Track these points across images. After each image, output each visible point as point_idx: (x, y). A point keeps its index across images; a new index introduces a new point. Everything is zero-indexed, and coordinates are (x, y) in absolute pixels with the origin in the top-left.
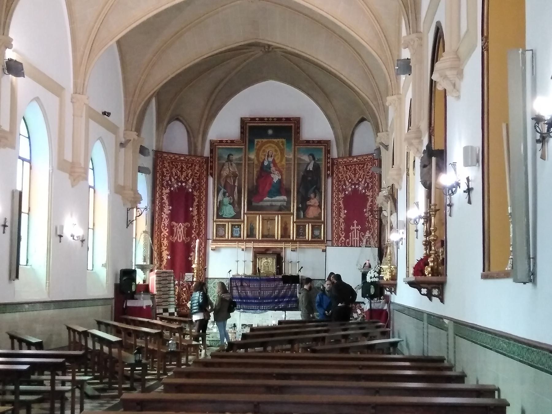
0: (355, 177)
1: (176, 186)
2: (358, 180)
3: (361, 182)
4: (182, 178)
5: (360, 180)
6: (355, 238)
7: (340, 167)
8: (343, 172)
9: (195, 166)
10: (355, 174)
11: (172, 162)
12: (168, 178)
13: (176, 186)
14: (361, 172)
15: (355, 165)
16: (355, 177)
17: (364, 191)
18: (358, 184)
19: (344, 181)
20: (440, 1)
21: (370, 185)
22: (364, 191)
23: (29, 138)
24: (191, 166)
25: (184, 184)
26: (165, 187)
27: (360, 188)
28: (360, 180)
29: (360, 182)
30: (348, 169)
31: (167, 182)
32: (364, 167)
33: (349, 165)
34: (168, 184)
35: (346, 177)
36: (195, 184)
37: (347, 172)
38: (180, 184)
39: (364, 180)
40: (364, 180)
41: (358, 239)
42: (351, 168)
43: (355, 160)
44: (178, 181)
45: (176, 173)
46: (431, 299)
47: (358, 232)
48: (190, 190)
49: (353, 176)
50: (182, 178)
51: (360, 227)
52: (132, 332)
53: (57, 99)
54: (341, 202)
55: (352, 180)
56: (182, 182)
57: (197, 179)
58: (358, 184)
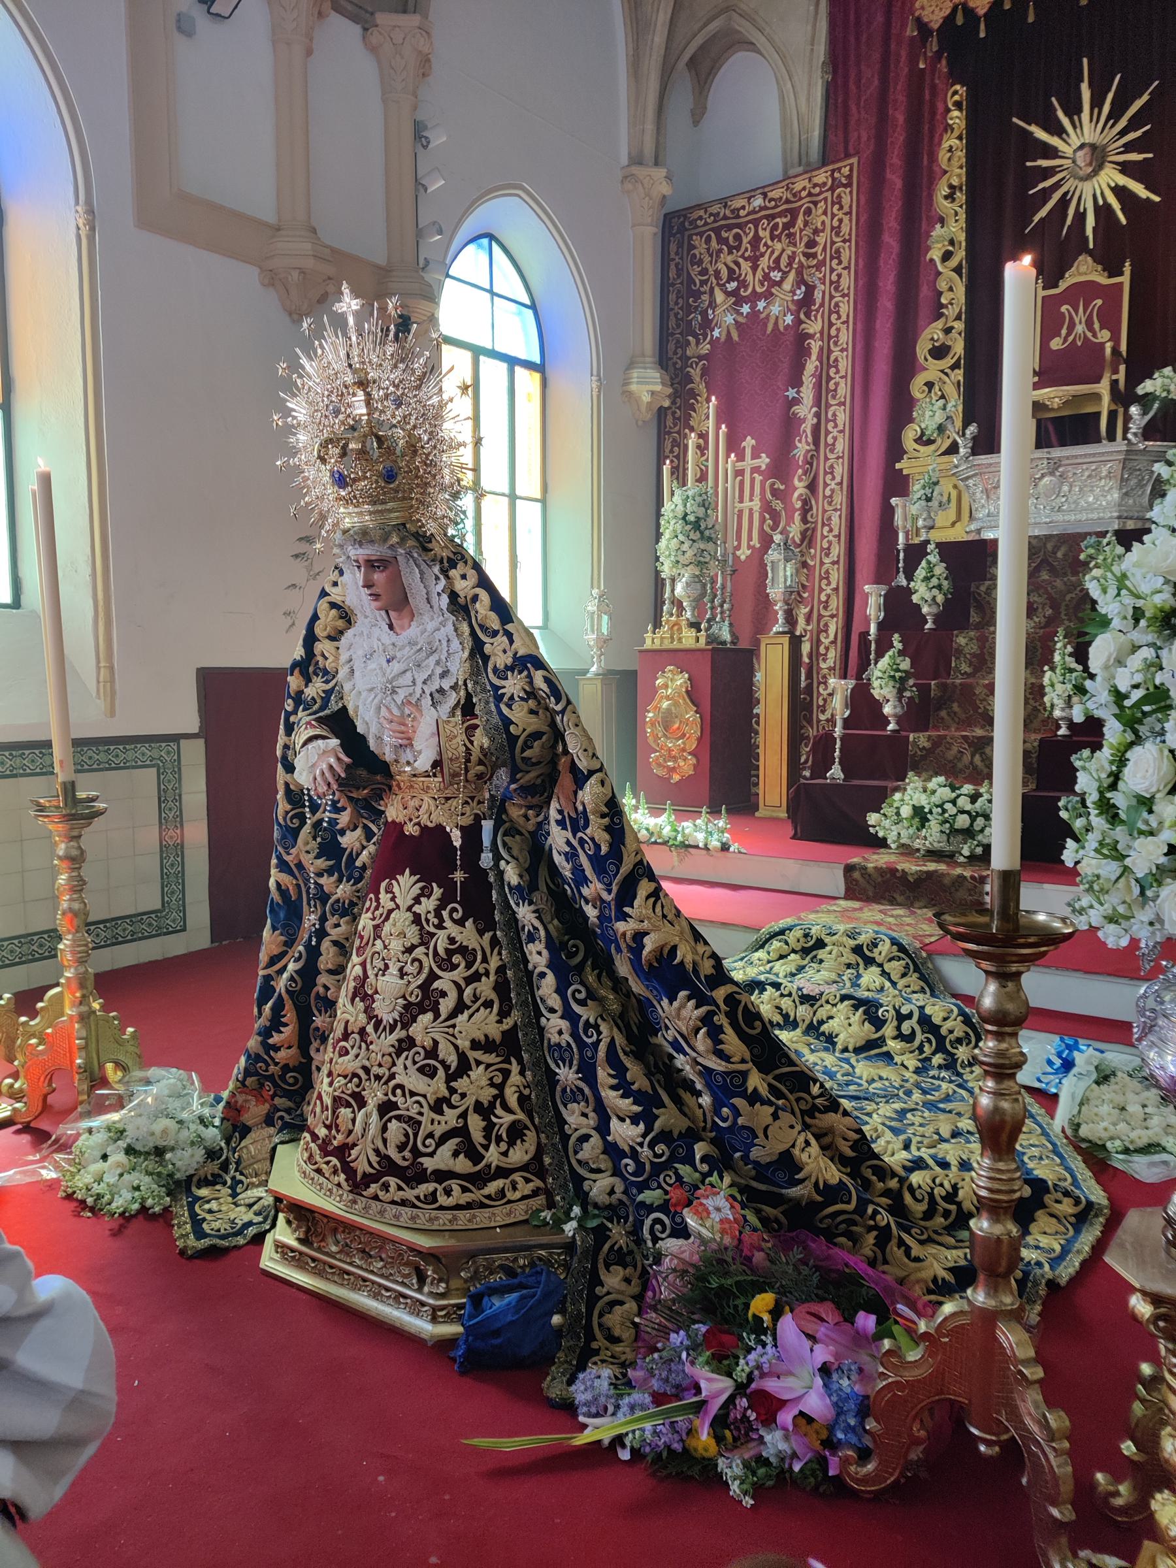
0: (755, 268)
2: (766, 277)
3: (779, 284)
5: (776, 275)
6: (747, 503)
7: (696, 240)
8: (707, 259)
10: (754, 261)
13: (729, 319)
14: (778, 246)
15: (756, 223)
16: (755, 268)
17: (789, 319)
21: (818, 295)
25: (761, 305)
26: (696, 336)
30: (725, 241)
32: (792, 223)
33: (729, 228)
35: (717, 273)
37: (720, 251)
39: (792, 276)
40: (792, 276)
41: (756, 504)
42: (738, 237)
43: (758, 202)
45: (731, 271)
47: (758, 478)
49: (746, 266)
50: (754, 282)
51: (764, 461)
52: (1036, 737)
55: (743, 284)
56: (755, 297)
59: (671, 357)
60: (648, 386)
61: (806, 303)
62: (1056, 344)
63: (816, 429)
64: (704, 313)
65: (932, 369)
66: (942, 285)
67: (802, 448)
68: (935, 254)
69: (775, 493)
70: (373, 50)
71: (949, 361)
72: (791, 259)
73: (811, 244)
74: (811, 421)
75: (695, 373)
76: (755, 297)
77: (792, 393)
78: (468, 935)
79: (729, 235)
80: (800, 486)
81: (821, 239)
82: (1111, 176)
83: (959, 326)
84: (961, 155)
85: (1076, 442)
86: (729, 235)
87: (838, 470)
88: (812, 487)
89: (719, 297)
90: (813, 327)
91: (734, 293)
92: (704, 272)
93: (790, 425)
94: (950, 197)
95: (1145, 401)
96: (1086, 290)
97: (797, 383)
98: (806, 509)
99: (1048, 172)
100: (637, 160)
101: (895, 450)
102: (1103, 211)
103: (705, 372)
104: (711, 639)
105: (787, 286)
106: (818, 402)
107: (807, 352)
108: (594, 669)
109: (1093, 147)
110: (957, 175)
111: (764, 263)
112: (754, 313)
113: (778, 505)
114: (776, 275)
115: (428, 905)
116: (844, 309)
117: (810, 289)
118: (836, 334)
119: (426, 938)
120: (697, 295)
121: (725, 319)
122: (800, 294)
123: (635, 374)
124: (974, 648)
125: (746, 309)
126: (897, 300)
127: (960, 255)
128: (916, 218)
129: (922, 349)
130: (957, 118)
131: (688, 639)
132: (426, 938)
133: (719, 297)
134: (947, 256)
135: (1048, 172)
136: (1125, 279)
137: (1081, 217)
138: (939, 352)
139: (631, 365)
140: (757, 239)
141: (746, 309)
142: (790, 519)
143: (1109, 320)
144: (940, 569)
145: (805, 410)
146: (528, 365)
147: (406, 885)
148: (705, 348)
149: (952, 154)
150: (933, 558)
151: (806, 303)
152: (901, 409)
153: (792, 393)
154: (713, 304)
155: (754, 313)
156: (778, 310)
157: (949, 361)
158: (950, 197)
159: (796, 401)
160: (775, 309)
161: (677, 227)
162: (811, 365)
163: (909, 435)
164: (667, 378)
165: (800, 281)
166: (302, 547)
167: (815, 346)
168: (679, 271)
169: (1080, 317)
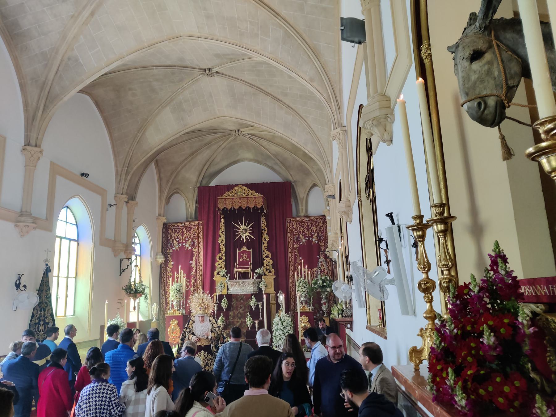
1: (304, 241)
2: (185, 239)
4: (308, 234)
5: (187, 239)
9: (319, 223)
11: (175, 229)
12: (297, 236)
13: (304, 241)
15: (183, 229)
17: (190, 248)
18: (185, 243)
19: (299, 235)
20: (380, 2)
21: (196, 244)
22: (317, 242)
23: (77, 225)
24: (316, 224)
25: (184, 244)
27: (187, 246)
28: (313, 233)
29: (187, 241)
31: (297, 239)
32: (190, 230)
34: (297, 240)
35: (174, 237)
36: (320, 237)
38: (307, 239)
43: (183, 225)
44: (305, 236)
46: (17, 289)
48: (317, 242)
49: (180, 236)
50: (182, 240)
53: (506, 119)
54: (296, 251)
55: (180, 240)
56: (182, 243)
57: (322, 233)
58: (312, 237)
59: (165, 253)
60: (161, 259)
61: (194, 245)
62: (241, 260)
63: (196, 270)
64: (171, 244)
65: (220, 262)
66: (221, 247)
67: (193, 273)
68: (220, 242)
69: (187, 281)
70: (127, 206)
71: (222, 261)
72: (190, 236)
73: (194, 234)
74: (195, 268)
75: (169, 256)
76: (182, 243)
77: (191, 262)
78: (211, 357)
79: (177, 230)
80: (193, 281)
81: (196, 234)
82: (247, 234)
83: (224, 255)
84: (224, 226)
85: (245, 279)
86: (177, 230)
87: (201, 278)
88: (195, 281)
89: (175, 242)
90: (195, 250)
91: (178, 241)
92: (171, 236)
93: (190, 269)
94: (222, 233)
95: (256, 273)
96: (244, 252)
97: (192, 260)
98: (194, 286)
99: (238, 232)
100: (159, 215)
101: (212, 276)
102: (242, 223)
103: (171, 256)
104: (182, 314)
105: (190, 241)
106: (196, 264)
107: (194, 254)
108: (154, 320)
109: (245, 229)
110: (223, 229)
111: (184, 236)
112: (182, 246)
113: (188, 284)
114: (187, 239)
115: (205, 354)
116: (201, 248)
117: (194, 243)
118: (199, 252)
119: (206, 358)
120: (170, 240)
121: (176, 246)
122: (192, 243)
123: (158, 256)
124: (233, 315)
125: (181, 245)
126: (212, 250)
127: (224, 243)
128: (215, 236)
129: (217, 258)
130: (223, 220)
131: (178, 314)
132: (206, 358)
133: (175, 242)
134: (222, 242)
135: (238, 232)
136: (251, 251)
137: (243, 239)
138: (221, 259)
139: (157, 255)
140: (183, 232)
141: (181, 245)
142: (191, 287)
143: (249, 257)
144: (226, 301)
145: (194, 265)
146: (139, 255)
147: (202, 352)
148: (171, 251)
149: (222, 225)
150: (225, 298)
151: (194, 245)
152: (213, 268)
153: (191, 262)
154: (173, 242)
155: (182, 246)
156: (188, 246)
157: (222, 261)
158: (222, 233)
159: (192, 264)
160: (187, 246)
161: (166, 226)
162: (195, 257)
163: (215, 273)
164: (291, 340)
165: (192, 241)
166: (120, 301)
167: (195, 254)
168: (165, 235)
169: (244, 256)
